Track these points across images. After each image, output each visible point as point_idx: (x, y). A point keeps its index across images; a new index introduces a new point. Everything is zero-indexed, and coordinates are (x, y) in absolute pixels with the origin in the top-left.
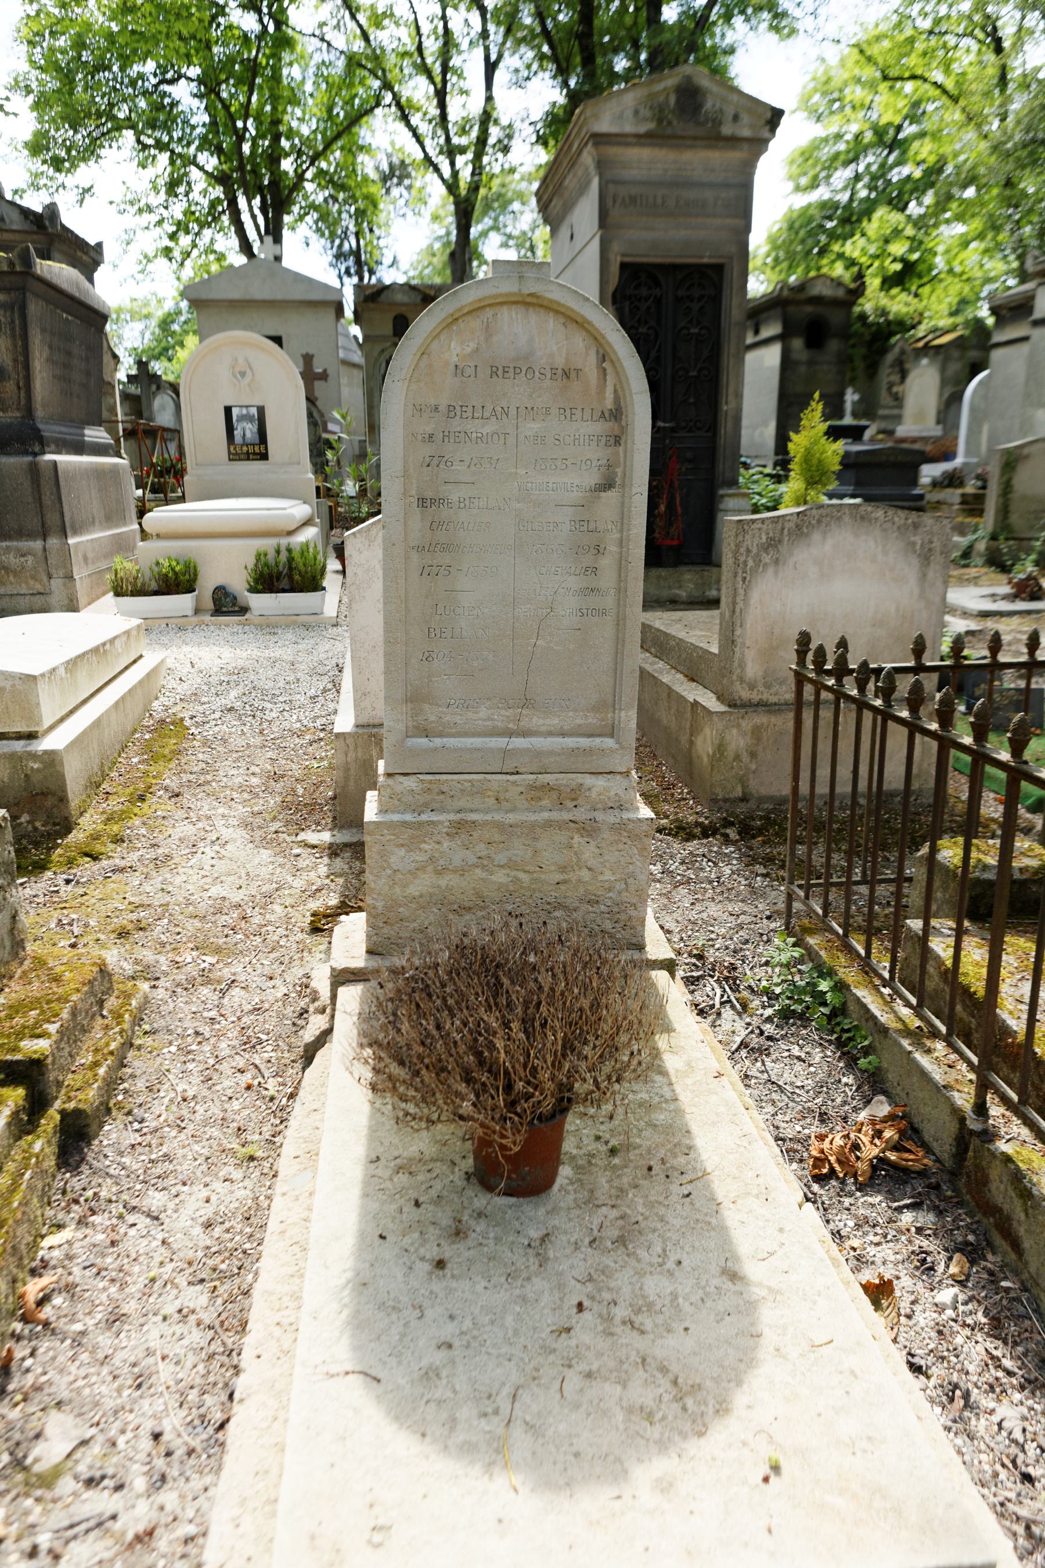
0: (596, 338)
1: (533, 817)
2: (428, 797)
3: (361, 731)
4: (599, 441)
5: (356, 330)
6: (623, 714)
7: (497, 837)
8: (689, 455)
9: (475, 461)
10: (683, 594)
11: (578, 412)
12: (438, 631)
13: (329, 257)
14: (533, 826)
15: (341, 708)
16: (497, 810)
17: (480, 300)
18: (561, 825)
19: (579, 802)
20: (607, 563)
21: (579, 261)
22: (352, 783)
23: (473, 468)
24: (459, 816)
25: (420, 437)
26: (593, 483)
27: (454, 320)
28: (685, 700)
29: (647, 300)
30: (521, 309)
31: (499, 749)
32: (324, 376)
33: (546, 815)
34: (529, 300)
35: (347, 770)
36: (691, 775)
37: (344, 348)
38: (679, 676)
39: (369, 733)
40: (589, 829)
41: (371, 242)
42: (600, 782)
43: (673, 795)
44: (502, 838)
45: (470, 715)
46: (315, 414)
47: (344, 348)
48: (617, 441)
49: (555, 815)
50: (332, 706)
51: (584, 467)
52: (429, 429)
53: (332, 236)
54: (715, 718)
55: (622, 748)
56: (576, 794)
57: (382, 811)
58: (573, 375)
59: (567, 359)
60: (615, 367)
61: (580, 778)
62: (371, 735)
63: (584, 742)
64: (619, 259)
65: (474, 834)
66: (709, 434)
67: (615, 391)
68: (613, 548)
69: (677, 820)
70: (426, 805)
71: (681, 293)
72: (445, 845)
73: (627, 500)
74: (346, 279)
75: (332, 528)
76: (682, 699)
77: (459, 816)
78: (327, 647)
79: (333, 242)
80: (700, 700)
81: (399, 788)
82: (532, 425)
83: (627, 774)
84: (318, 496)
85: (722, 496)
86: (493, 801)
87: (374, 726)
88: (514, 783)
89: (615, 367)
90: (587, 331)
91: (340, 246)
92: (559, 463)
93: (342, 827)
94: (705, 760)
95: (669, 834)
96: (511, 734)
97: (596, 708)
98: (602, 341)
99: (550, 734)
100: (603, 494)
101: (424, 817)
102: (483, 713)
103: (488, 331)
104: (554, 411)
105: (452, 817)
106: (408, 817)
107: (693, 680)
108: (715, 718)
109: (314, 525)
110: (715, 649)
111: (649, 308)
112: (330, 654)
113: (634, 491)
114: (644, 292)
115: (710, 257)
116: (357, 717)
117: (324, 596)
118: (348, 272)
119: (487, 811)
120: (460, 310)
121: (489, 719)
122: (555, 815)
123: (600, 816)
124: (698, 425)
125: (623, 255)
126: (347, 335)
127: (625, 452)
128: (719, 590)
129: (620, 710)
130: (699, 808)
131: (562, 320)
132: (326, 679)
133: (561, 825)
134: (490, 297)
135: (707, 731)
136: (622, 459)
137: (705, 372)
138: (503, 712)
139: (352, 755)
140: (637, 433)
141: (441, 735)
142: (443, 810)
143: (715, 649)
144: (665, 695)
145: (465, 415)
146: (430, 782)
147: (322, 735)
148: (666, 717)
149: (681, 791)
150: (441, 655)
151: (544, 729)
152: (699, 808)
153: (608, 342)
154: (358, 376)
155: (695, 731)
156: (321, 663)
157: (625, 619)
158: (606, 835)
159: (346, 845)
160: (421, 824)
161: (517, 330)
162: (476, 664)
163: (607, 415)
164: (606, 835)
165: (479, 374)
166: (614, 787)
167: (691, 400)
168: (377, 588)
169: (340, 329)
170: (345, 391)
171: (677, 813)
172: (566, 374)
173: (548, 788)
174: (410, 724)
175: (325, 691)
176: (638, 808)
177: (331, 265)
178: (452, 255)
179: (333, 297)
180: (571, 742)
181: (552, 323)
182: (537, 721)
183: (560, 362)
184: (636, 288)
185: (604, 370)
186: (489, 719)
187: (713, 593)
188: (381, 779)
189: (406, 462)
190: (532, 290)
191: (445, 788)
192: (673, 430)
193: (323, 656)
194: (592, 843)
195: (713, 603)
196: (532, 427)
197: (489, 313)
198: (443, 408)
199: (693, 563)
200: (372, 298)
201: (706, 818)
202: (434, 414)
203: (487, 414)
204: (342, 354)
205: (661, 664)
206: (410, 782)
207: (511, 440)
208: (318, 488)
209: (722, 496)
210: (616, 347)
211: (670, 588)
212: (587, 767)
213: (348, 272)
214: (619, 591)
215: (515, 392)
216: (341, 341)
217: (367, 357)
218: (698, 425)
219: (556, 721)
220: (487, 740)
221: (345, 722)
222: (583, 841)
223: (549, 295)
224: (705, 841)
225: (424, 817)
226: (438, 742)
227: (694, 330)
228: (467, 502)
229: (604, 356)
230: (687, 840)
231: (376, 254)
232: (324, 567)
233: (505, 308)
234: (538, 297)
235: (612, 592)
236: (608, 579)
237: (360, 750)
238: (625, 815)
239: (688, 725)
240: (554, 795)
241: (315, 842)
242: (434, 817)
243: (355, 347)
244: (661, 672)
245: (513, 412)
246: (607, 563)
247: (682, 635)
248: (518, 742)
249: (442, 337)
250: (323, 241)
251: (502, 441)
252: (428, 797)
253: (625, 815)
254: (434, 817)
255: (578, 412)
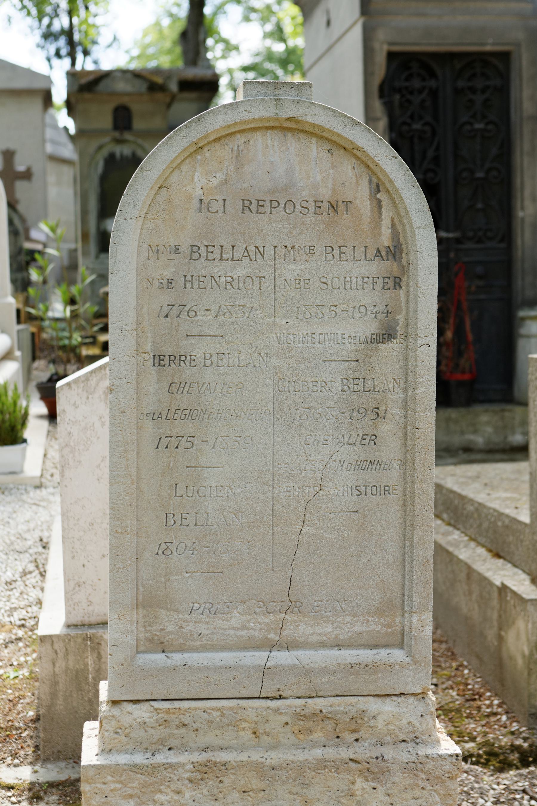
0: (368, 166)
1: (301, 756)
2: (164, 731)
3: (73, 632)
4: (374, 283)
5: (65, 120)
6: (415, 618)
7: (256, 784)
8: (479, 270)
9: (224, 309)
10: (479, 440)
11: (349, 251)
12: (178, 517)
13: (37, 37)
14: (302, 767)
15: (47, 598)
16: (254, 747)
17: (229, 126)
18: (339, 766)
19: (362, 734)
20: (388, 429)
21: (338, 49)
22: (60, 701)
23: (221, 318)
24: (205, 756)
25: (156, 283)
26: (368, 333)
27: (199, 148)
28: (491, 584)
29: (420, 91)
30: (278, 135)
31: (257, 667)
32: (27, 175)
33: (318, 753)
34: (287, 124)
35: (55, 683)
36: (502, 681)
37: (53, 142)
38: (481, 551)
39: (85, 633)
40: (374, 770)
41: (86, 20)
42: (388, 707)
43: (479, 708)
44: (262, 785)
45: (219, 623)
46: (17, 221)
47: (53, 142)
48: (397, 283)
49: (330, 753)
50: (34, 594)
51: (357, 315)
52: (167, 274)
53: (40, 16)
54: (530, 608)
55: (415, 662)
56: (356, 724)
57: (106, 750)
58: (341, 208)
59: (334, 190)
60: (392, 198)
61: (361, 703)
62: (86, 638)
63: (366, 655)
64: (386, 48)
65: (226, 779)
66: (503, 245)
67: (393, 225)
68: (396, 411)
69: (487, 743)
70: (162, 742)
71: (461, 84)
72: (188, 794)
73: (411, 353)
74: (55, 61)
75: (34, 358)
76: (484, 581)
77: (205, 756)
78: (28, 515)
79: (40, 20)
80: (509, 583)
81: (126, 720)
82: (293, 266)
83: (423, 695)
84: (19, 322)
85: (523, 319)
86: (249, 735)
87: (90, 626)
88: (277, 710)
89: (392, 198)
90: (357, 158)
91: (49, 25)
92: (326, 310)
93: (46, 760)
94: (520, 662)
95: (477, 763)
96: (271, 646)
97: (380, 611)
98: (376, 169)
99: (322, 645)
100: (381, 346)
101: (160, 758)
102: (236, 619)
103: (239, 160)
104: (320, 250)
105: (196, 757)
106: (139, 759)
107: (498, 556)
108: (530, 608)
109: (14, 359)
110: (525, 517)
111: (423, 101)
112: (32, 525)
113: (420, 342)
114: (416, 83)
115: (494, 44)
116: (68, 613)
117: (24, 450)
118: (58, 54)
119: (242, 748)
120: (205, 137)
121: (243, 627)
122: (330, 753)
123: (389, 752)
124: (489, 234)
125: (390, 44)
126: (55, 126)
127: (408, 296)
128: (526, 433)
129: (411, 612)
130: (515, 727)
131: (327, 146)
132: (26, 557)
133: (339, 766)
134: (241, 123)
135: (520, 624)
136: (403, 305)
137: (494, 173)
138: (260, 618)
139: (61, 664)
140: (420, 274)
141: (181, 650)
142: (184, 748)
143: (525, 517)
144: (463, 576)
145: (211, 256)
146: (168, 711)
147: (20, 633)
148: (466, 603)
149: (490, 702)
150: (182, 546)
151: (313, 639)
152: (515, 727)
153: (382, 170)
154: (68, 173)
155: (504, 623)
156: (20, 537)
157: (413, 497)
158: (398, 777)
159: (52, 785)
160: (154, 767)
161: (274, 159)
162: (225, 557)
163: (384, 253)
164: (398, 777)
165: (229, 209)
166: (407, 713)
167: (480, 206)
168: (100, 447)
169: (48, 120)
170: (53, 192)
171: (485, 734)
172: (333, 207)
173: (320, 716)
174: (142, 636)
175: (25, 573)
176: (438, 741)
177: (38, 46)
178: (184, 35)
179: (40, 85)
180: (348, 655)
181: (314, 149)
182: (304, 630)
183: (325, 194)
184: (407, 80)
185: (379, 201)
186: (243, 627)
187: (517, 439)
188: (104, 708)
189: (139, 312)
190: (291, 114)
191: (187, 720)
192: (458, 241)
193: (22, 528)
194: (380, 789)
195: (520, 452)
196: (293, 269)
197: (240, 140)
198: (185, 249)
199: (490, 401)
200: (87, 88)
201: (525, 739)
202: (174, 256)
203: (238, 255)
204: (49, 148)
205: (456, 535)
206: (141, 712)
207: (268, 284)
208: (18, 311)
209: (523, 319)
210: (393, 176)
211: (462, 433)
212: (371, 688)
213: (58, 54)
214: (405, 463)
215: (273, 229)
216: (49, 133)
217: (81, 154)
218: (489, 234)
219: (329, 628)
220: (241, 654)
221: (53, 621)
222: (368, 786)
223: (310, 120)
224: (524, 771)
225: (160, 758)
226: (177, 658)
227: (479, 126)
228: (214, 359)
229: (378, 187)
230: (501, 770)
231: (92, 32)
232: (25, 416)
233: (259, 134)
234: (298, 122)
235: (396, 464)
236: (390, 449)
237: (71, 658)
238: (423, 751)
239: (495, 616)
240: (329, 725)
241: (11, 781)
242: (173, 758)
243: (65, 139)
244: (456, 544)
245: (269, 252)
246: (388, 429)
247: (481, 497)
248: (281, 657)
249: (184, 168)
250: (29, 20)
251: (257, 286)
252: (164, 731)
253: (423, 751)
254: (173, 758)
255: (349, 251)
